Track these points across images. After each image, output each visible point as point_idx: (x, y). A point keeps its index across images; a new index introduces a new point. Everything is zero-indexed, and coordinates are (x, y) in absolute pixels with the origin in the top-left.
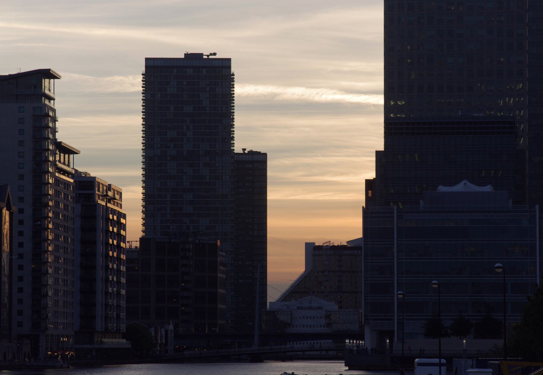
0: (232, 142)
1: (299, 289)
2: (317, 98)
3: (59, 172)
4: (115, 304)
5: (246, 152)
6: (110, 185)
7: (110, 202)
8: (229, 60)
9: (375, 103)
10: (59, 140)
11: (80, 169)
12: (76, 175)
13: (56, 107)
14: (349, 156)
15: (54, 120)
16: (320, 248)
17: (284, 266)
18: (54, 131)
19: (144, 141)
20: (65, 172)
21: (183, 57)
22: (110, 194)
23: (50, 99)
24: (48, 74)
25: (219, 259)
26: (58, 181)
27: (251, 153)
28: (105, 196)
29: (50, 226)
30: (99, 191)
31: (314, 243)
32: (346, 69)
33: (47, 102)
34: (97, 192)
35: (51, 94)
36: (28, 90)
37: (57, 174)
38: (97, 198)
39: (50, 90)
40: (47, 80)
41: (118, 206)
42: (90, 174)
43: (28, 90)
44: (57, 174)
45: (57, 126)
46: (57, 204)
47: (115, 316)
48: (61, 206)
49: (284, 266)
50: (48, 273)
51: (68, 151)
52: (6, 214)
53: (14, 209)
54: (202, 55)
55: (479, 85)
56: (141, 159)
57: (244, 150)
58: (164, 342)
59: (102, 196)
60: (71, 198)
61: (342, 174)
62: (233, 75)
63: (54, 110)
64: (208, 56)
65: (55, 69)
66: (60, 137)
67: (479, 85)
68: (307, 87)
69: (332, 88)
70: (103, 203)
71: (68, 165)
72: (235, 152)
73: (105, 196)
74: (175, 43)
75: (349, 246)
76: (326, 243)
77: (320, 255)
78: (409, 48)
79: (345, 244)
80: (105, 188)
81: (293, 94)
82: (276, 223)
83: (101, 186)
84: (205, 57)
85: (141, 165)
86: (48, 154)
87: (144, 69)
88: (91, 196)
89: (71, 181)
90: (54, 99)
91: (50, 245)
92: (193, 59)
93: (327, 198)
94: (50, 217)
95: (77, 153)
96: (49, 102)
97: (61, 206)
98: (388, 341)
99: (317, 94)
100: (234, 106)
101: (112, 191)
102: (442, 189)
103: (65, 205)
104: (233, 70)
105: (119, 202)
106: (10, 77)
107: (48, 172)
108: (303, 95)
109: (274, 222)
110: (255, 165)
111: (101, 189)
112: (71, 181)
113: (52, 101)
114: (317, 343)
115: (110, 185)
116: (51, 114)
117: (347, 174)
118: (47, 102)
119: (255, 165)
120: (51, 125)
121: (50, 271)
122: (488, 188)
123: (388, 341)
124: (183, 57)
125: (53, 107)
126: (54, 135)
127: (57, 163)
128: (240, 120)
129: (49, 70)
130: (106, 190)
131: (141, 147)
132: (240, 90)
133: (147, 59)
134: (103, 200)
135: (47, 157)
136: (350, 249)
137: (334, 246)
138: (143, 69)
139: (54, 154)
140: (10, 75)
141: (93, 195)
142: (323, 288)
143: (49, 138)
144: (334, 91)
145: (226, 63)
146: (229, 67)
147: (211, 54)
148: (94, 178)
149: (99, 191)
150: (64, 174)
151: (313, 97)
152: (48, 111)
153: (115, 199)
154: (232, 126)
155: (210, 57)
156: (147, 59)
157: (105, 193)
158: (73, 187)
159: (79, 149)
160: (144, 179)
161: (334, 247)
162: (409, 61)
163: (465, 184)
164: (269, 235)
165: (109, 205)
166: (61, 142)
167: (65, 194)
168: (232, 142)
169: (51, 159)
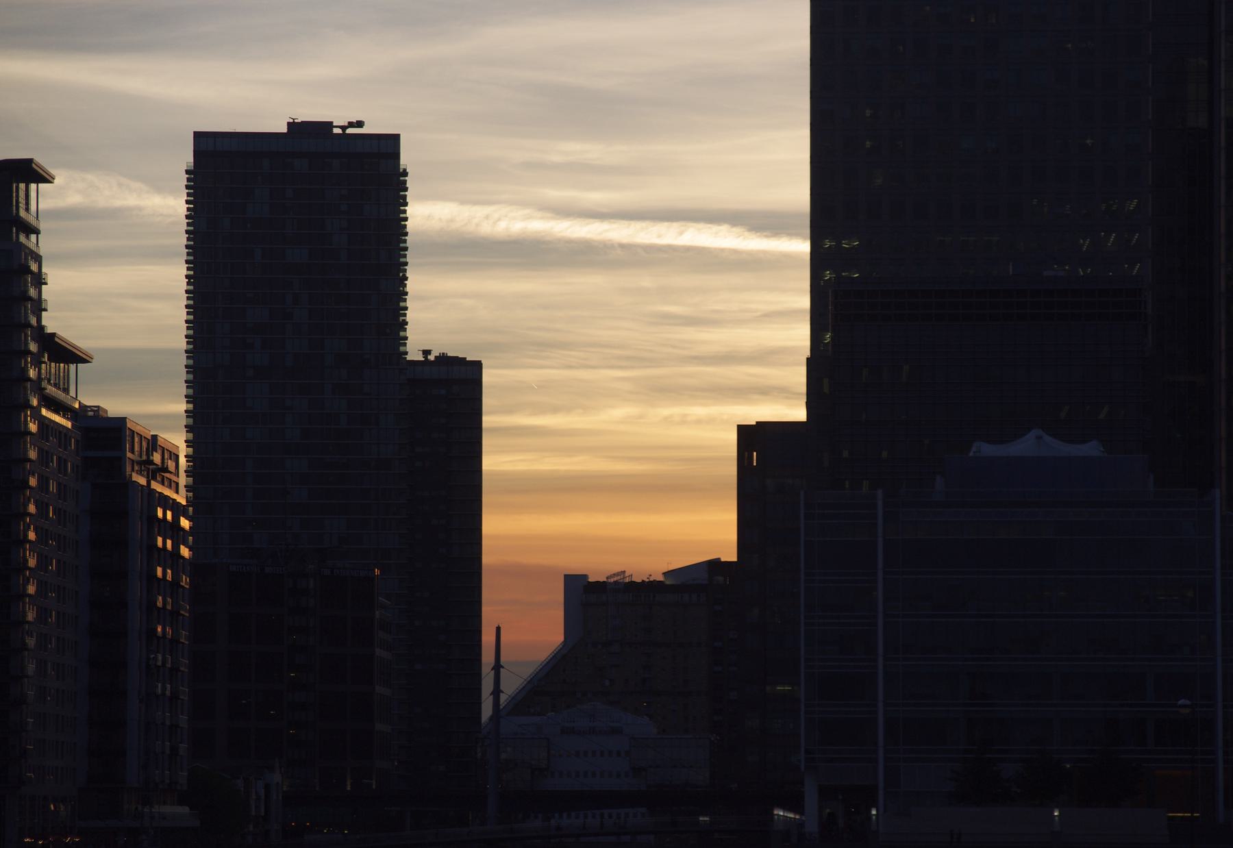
0: (402, 334)
3: (48, 408)
4: (168, 723)
5: (431, 358)
6: (155, 437)
7: (154, 479)
8: (395, 139)
9: (625, 241)
10: (49, 330)
14: (570, 367)
16: (600, 587)
20: (58, 407)
21: (284, 130)
22: (157, 458)
26: (45, 424)
27: (443, 359)
28: (146, 466)
29: (32, 536)
31: (585, 576)
32: (556, 158)
33: (22, 238)
34: (129, 455)
35: (31, 219)
37: (44, 412)
38: (128, 469)
39: (27, 209)
40: (22, 186)
41: (170, 487)
42: (106, 411)
44: (44, 412)
45: (44, 297)
46: (43, 482)
47: (168, 752)
48: (53, 487)
49: (522, 628)
54: (329, 125)
56: (183, 375)
57: (426, 353)
59: (140, 463)
60: (72, 469)
61: (555, 410)
62: (405, 173)
64: (343, 128)
65: (42, 160)
66: (50, 322)
68: (463, 202)
69: (523, 204)
70: (142, 481)
71: (66, 390)
72: (409, 358)
73: (146, 466)
74: (262, 96)
75: (668, 583)
78: (868, 113)
79: (661, 578)
80: (144, 444)
81: (429, 217)
83: (136, 439)
84: (337, 131)
85: (183, 390)
86: (26, 362)
87: (191, 160)
88: (117, 464)
90: (37, 232)
91: (28, 582)
92: (308, 134)
93: (521, 467)
96: (28, 237)
97: (53, 487)
98: (874, 812)
99: (487, 217)
101: (160, 451)
102: (987, 450)
103: (59, 484)
104: (405, 160)
105: (174, 478)
107: (28, 405)
108: (452, 220)
109: (499, 526)
113: (33, 237)
114: (610, 817)
115: (155, 437)
118: (22, 238)
120: (32, 292)
121: (31, 642)
122: (1091, 449)
123: (874, 812)
124: (284, 130)
125: (34, 249)
126: (39, 319)
127: (44, 384)
128: (418, 282)
129: (30, 161)
130: (147, 449)
132: (423, 214)
134: (140, 473)
135: (25, 371)
137: (632, 583)
138: (187, 158)
139: (38, 363)
141: (121, 459)
142: (607, 683)
144: (527, 211)
146: (396, 155)
147: (351, 125)
148: (122, 421)
150: (56, 412)
151: (477, 225)
152: (26, 259)
153: (166, 470)
155: (350, 131)
156: (198, 136)
157: (144, 457)
158: (77, 442)
159: (90, 352)
160: (191, 421)
161: (632, 584)
162: (868, 144)
163: (1039, 438)
164: (487, 559)
165: (155, 486)
166: (53, 335)
167: (59, 459)
168: (402, 334)
169: (32, 373)
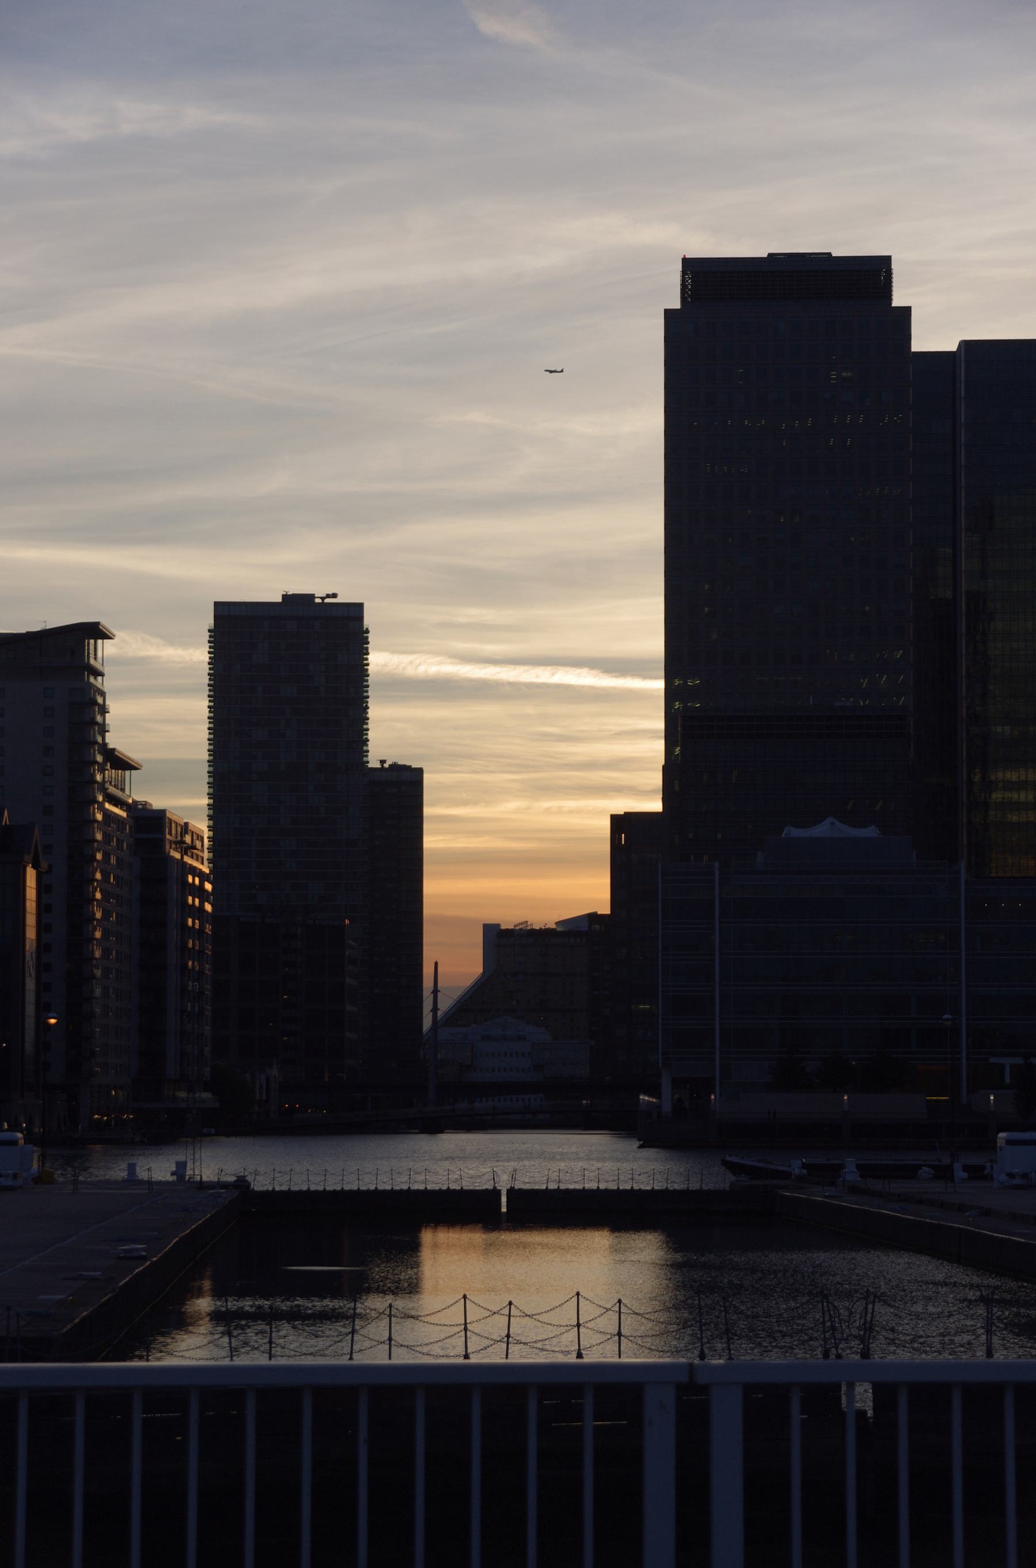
1: (476, 1002)
2: (410, 672)
3: (110, 803)
5: (386, 765)
6: (186, 824)
10: (111, 746)
11: (138, 799)
12: (132, 808)
13: (106, 688)
15: (104, 710)
16: (509, 933)
17: (452, 962)
18: (103, 730)
19: (212, 747)
21: (280, 600)
22: (188, 839)
23: (97, 673)
24: (95, 631)
25: (347, 953)
27: (395, 767)
28: (180, 844)
30: (171, 834)
31: (499, 925)
32: (462, 620)
34: (168, 836)
36: (60, 662)
38: (168, 847)
39: (95, 659)
40: (92, 641)
41: (197, 860)
43: (60, 662)
46: (106, 856)
48: (113, 860)
49: (452, 962)
50: (95, 978)
51: (122, 764)
52: (31, 875)
53: (44, 865)
54: (312, 597)
55: (828, 651)
57: (383, 762)
58: (264, 1098)
59: (176, 843)
61: (465, 803)
62: (367, 631)
63: (103, 694)
64: (323, 598)
65: (107, 623)
66: (113, 740)
67: (828, 651)
68: (393, 652)
69: (437, 653)
70: (178, 856)
71: (123, 790)
72: (370, 765)
73: (180, 844)
74: (264, 578)
76: (522, 924)
77: (510, 946)
78: (707, 587)
79: (554, 926)
80: (179, 829)
82: (437, 889)
83: (173, 825)
84: (318, 601)
85: (206, 789)
87: (212, 622)
88: (159, 844)
89: (124, 814)
90: (102, 675)
92: (297, 604)
93: (442, 845)
94: (97, 881)
95: (136, 769)
97: (113, 860)
99: (411, 663)
100: (368, 686)
103: (118, 859)
105: (200, 854)
106: (29, 635)
108: (385, 665)
110: (404, 786)
111: (173, 832)
112: (124, 814)
113: (100, 678)
115: (186, 824)
116: (100, 700)
117: (474, 803)
118: (92, 679)
119: (404, 786)
120: (99, 719)
124: (280, 600)
126: (104, 739)
129: (98, 623)
131: (205, 756)
132: (378, 661)
133: (217, 605)
134: (176, 850)
135: (93, 775)
136: (583, 930)
137: (533, 930)
138: (209, 621)
139: (102, 770)
140: (28, 633)
141: (162, 840)
142: (514, 1003)
143: (96, 743)
144: (440, 658)
145: (356, 611)
146: (360, 618)
147: (328, 596)
148: (162, 813)
149: (171, 834)
150: (116, 805)
151: (404, 669)
153: (195, 848)
154: (365, 719)
155: (327, 601)
156: (217, 605)
158: (130, 827)
159: (140, 762)
162: (706, 609)
164: (428, 910)
165: (187, 859)
166: (114, 750)
167: (118, 839)
